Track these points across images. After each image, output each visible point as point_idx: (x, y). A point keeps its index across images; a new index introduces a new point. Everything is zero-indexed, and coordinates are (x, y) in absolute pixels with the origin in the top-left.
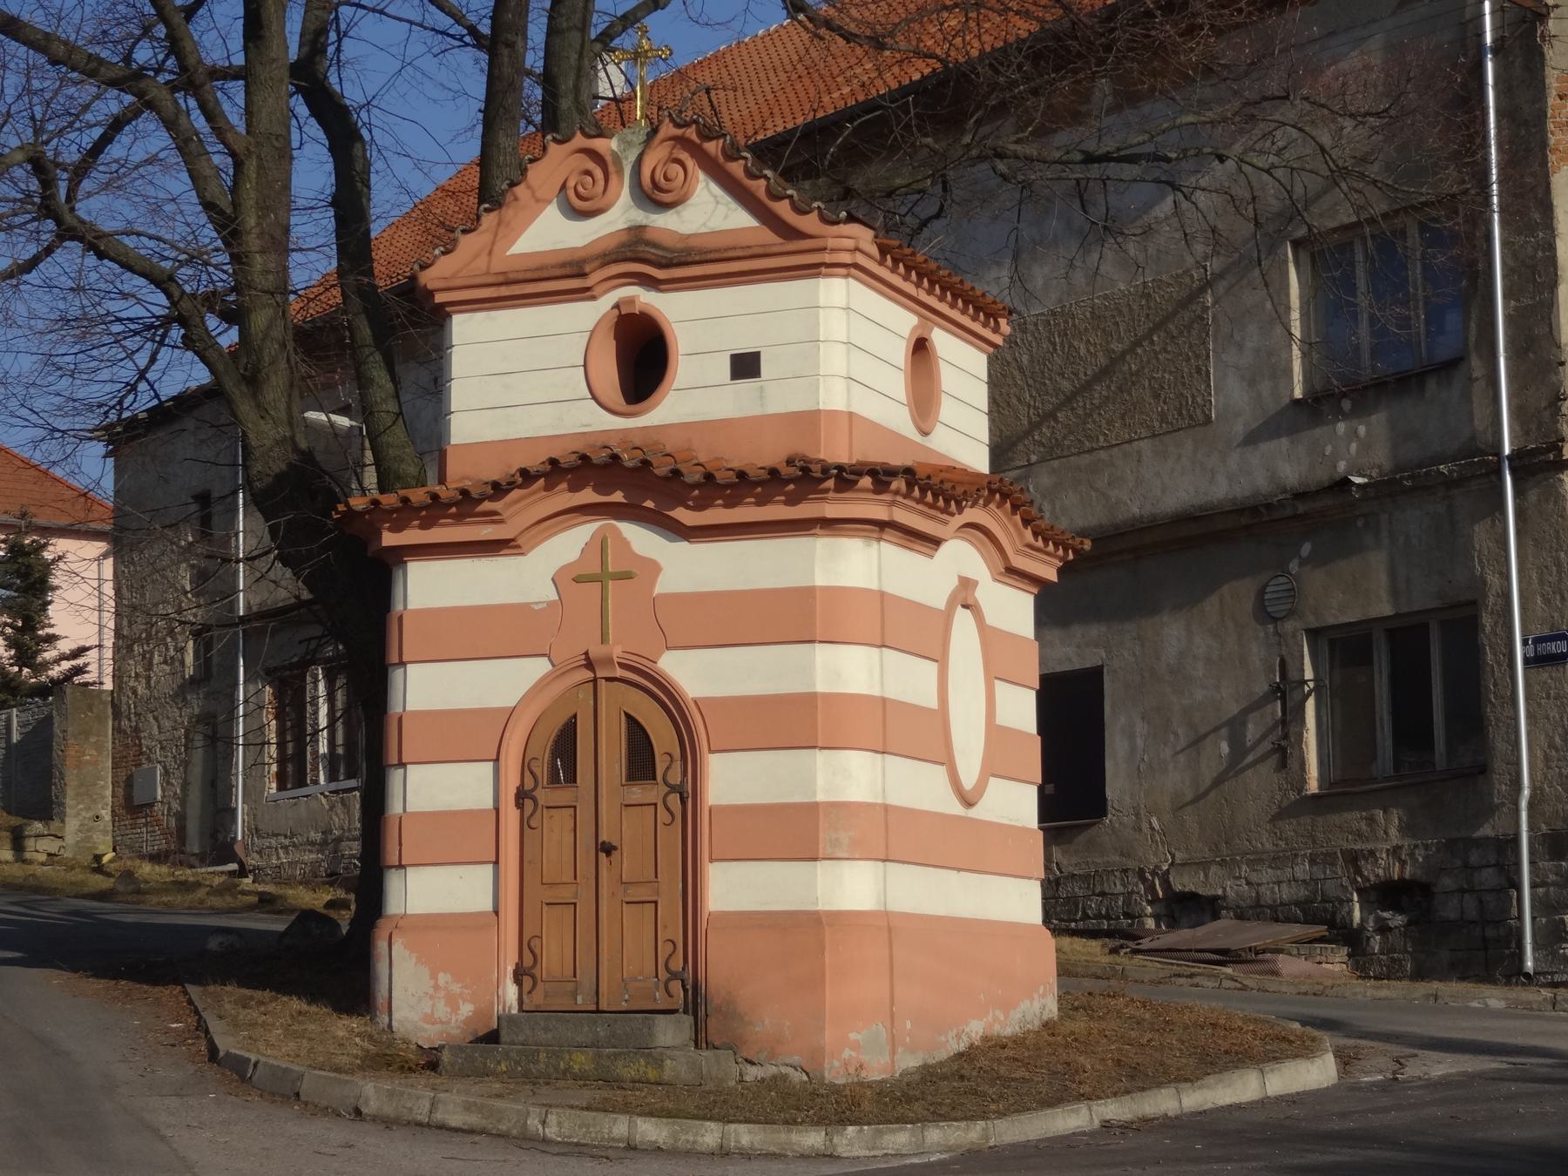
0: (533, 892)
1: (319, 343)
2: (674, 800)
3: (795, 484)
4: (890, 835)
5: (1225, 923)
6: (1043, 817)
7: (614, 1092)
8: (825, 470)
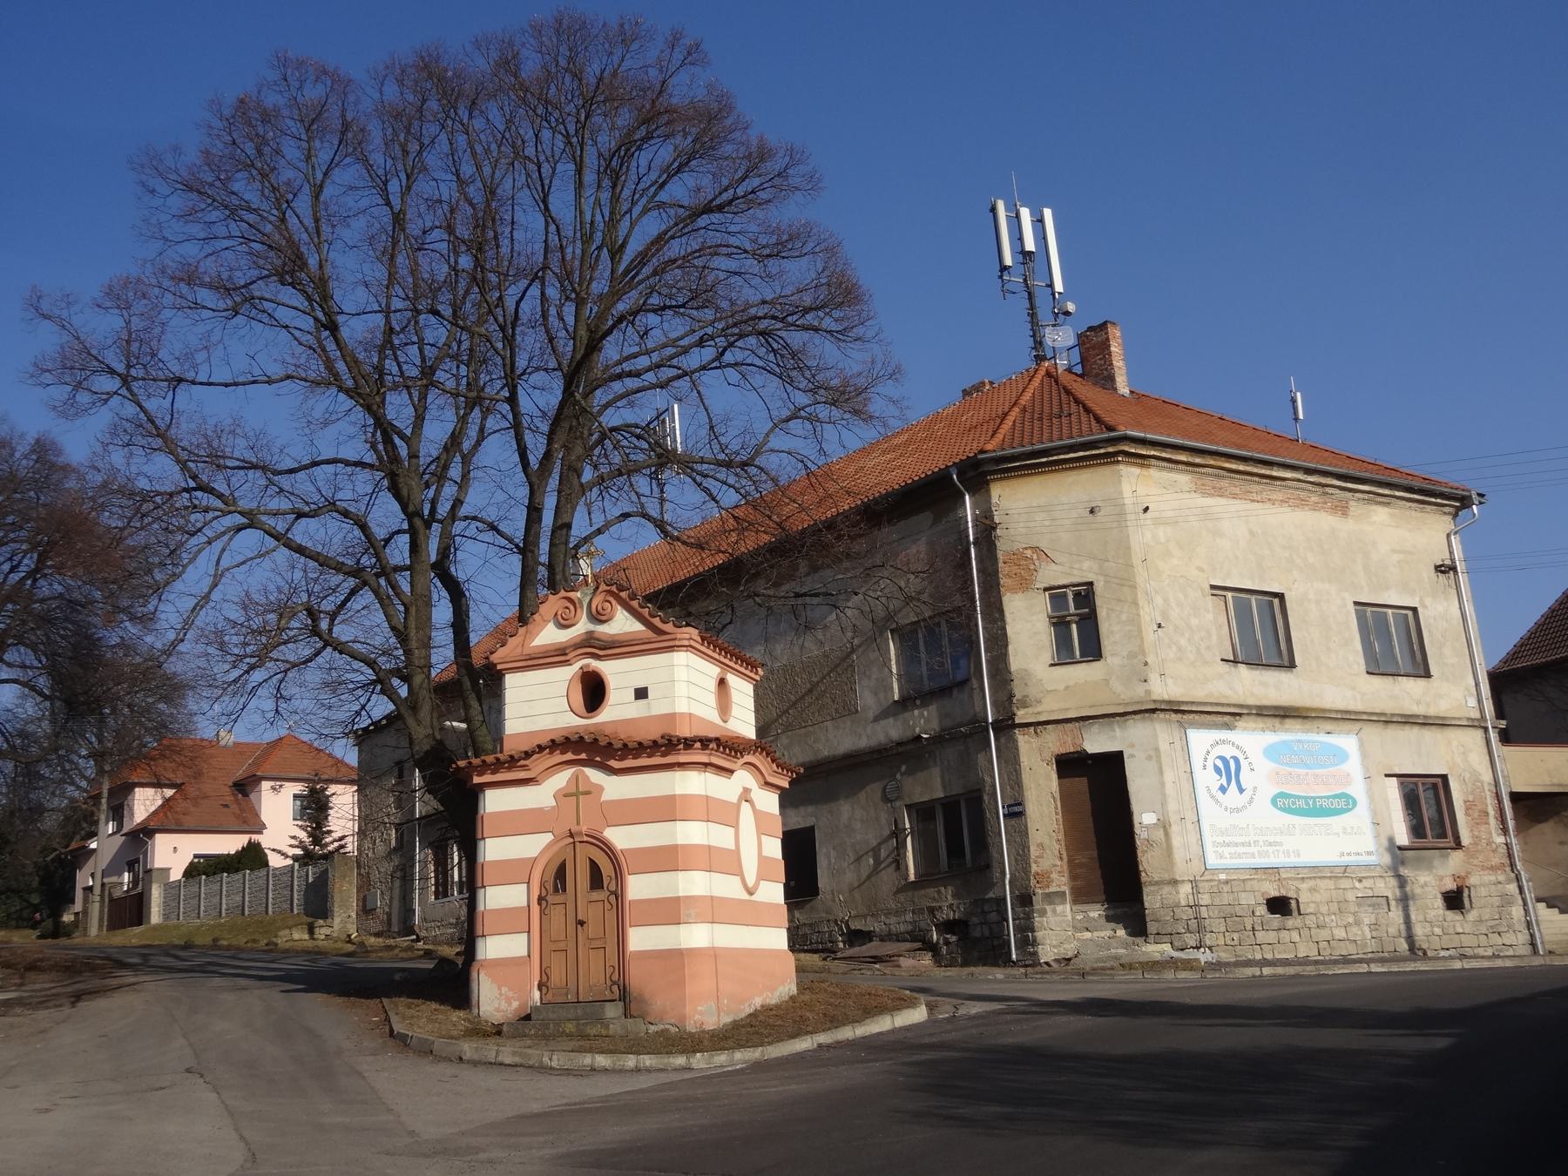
0: (547, 946)
1: (448, 693)
2: (613, 898)
3: (665, 747)
4: (715, 910)
5: (875, 943)
6: (786, 897)
7: (587, 1042)
8: (679, 740)
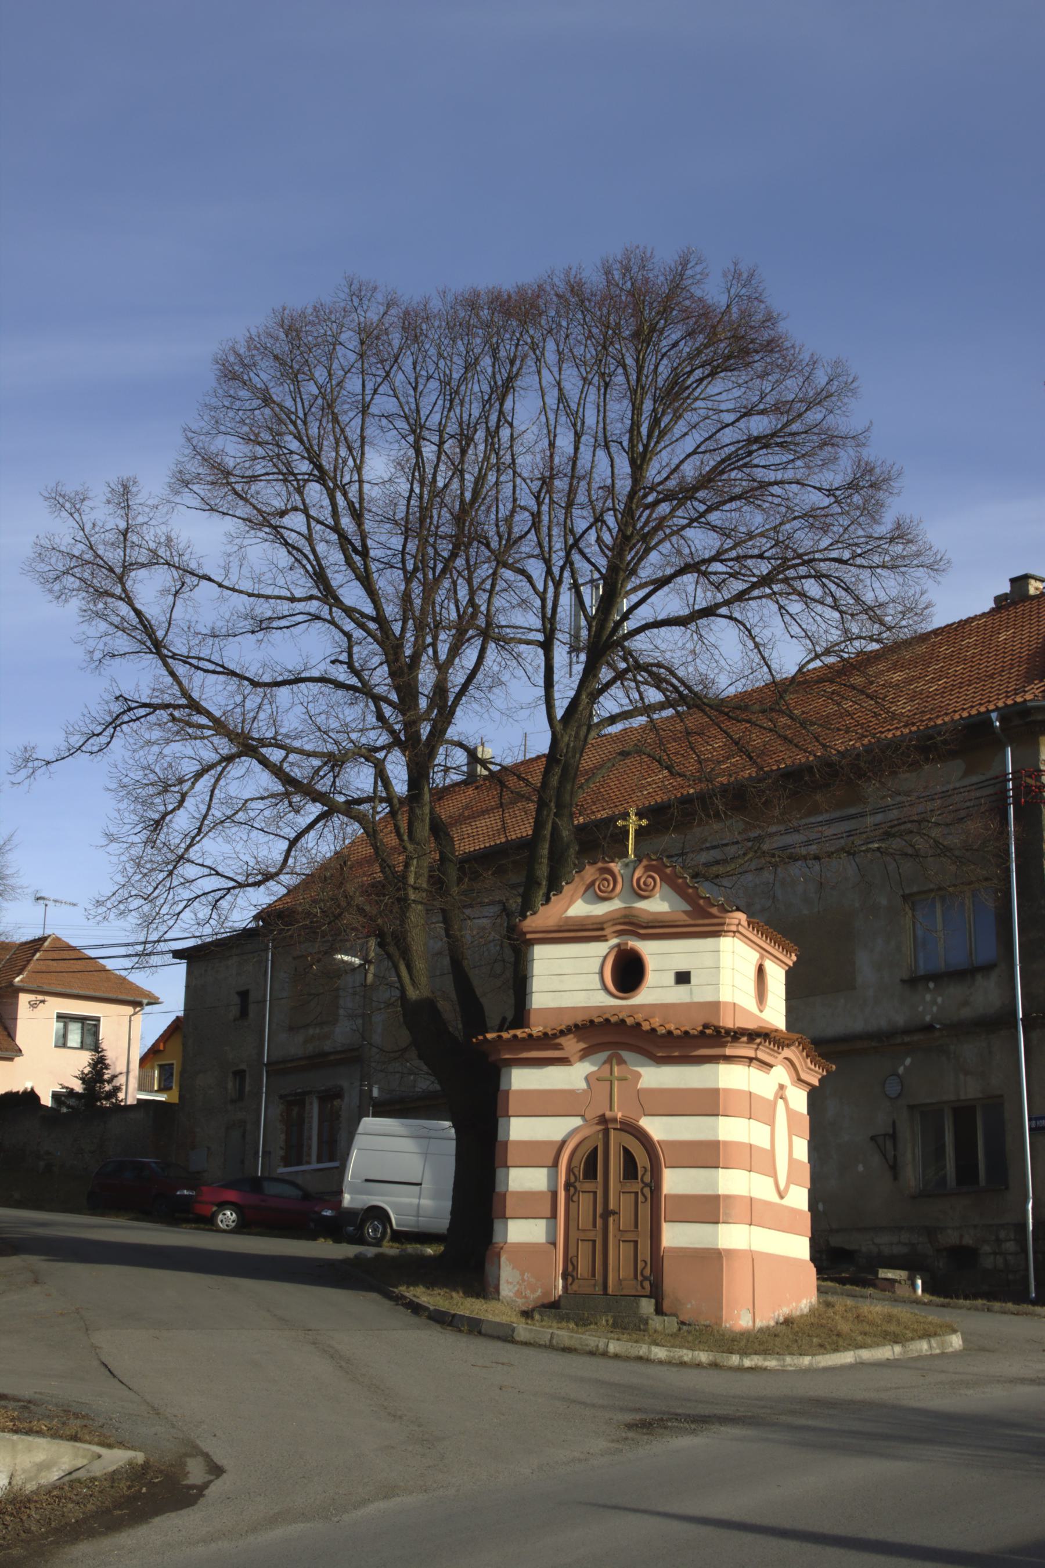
2: (647, 1191)
3: (707, 1038)
4: (753, 1212)
